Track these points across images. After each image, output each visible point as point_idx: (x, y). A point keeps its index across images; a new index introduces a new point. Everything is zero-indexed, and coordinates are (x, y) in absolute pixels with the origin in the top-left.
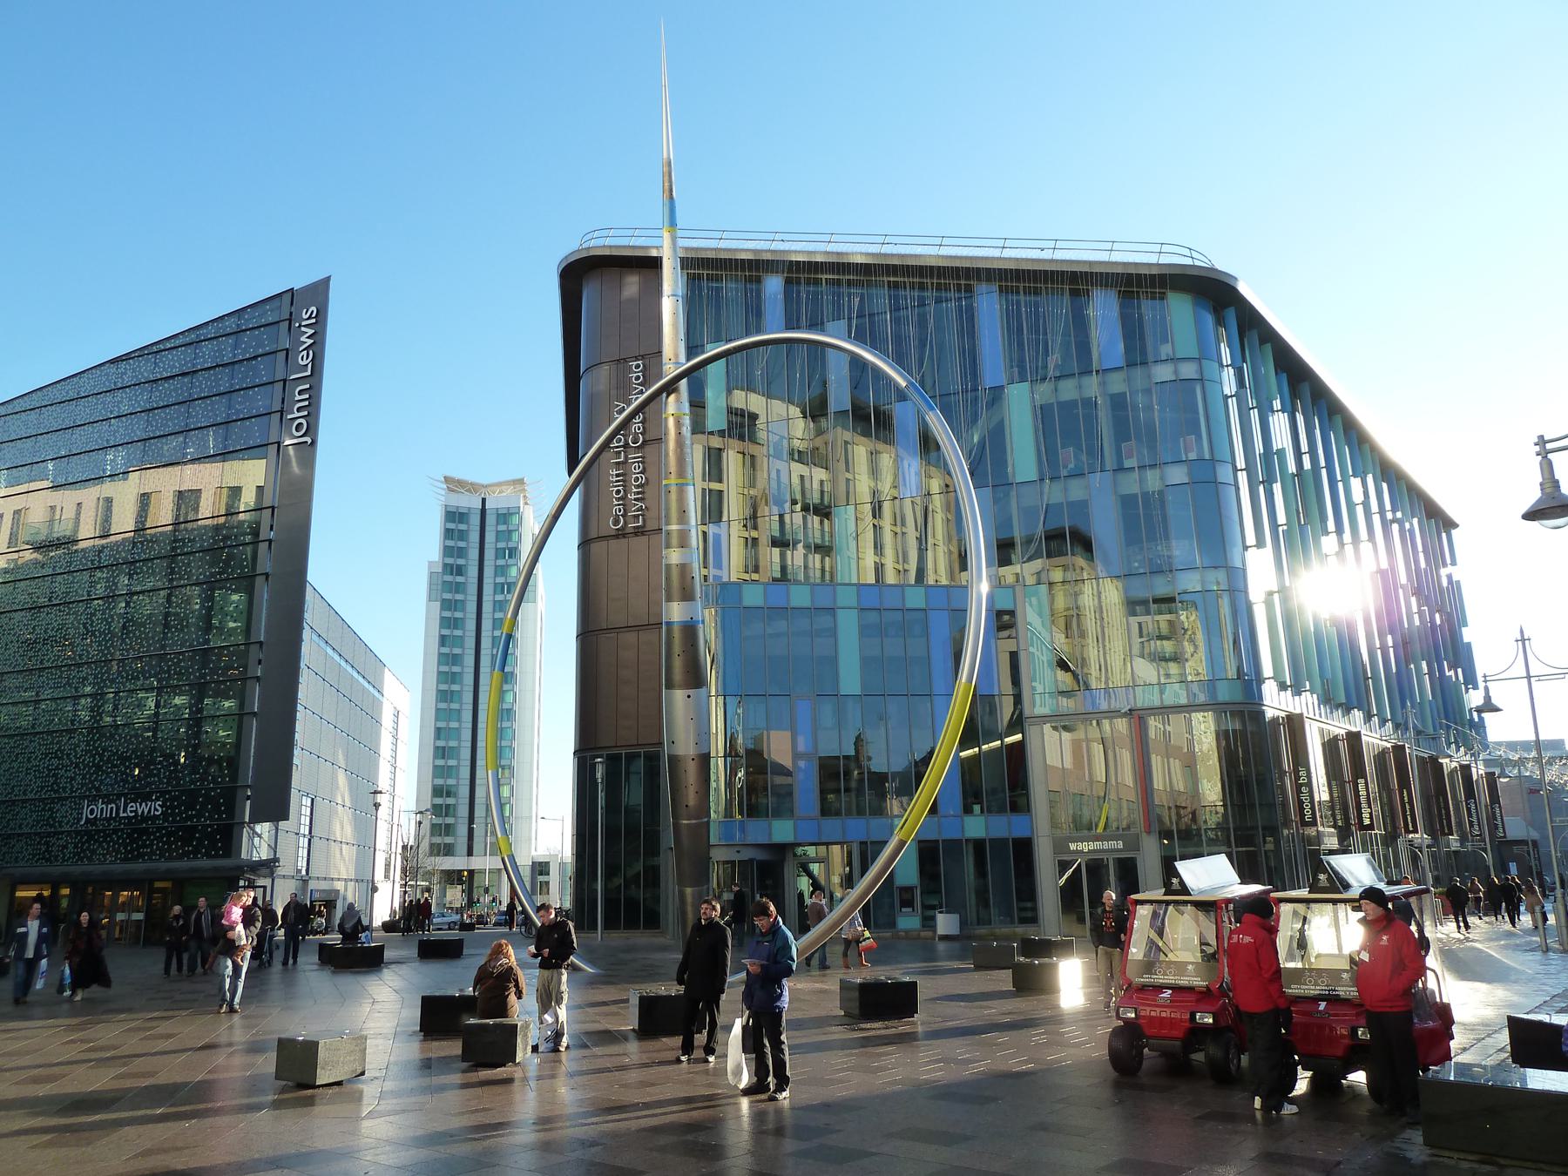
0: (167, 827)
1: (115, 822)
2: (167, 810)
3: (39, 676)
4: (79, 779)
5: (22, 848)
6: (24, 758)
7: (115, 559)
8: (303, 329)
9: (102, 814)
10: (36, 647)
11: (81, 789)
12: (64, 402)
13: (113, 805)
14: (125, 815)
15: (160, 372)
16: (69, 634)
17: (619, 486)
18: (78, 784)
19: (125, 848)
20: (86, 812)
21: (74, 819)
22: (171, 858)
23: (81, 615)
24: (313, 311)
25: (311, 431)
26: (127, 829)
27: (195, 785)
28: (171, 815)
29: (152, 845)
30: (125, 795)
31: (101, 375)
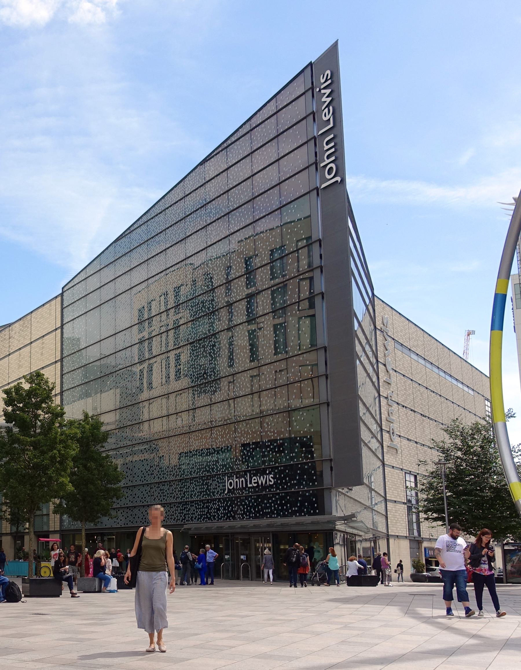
0: (278, 467)
1: (246, 491)
2: (277, 481)
10: (187, 485)
11: (223, 468)
12: (178, 222)
13: (243, 479)
14: (251, 485)
15: (235, 297)
16: (204, 453)
19: (254, 509)
20: (227, 484)
21: (221, 490)
22: (284, 516)
25: (340, 173)
26: (254, 496)
27: (294, 461)
28: (280, 484)
29: (271, 507)
31: (197, 218)
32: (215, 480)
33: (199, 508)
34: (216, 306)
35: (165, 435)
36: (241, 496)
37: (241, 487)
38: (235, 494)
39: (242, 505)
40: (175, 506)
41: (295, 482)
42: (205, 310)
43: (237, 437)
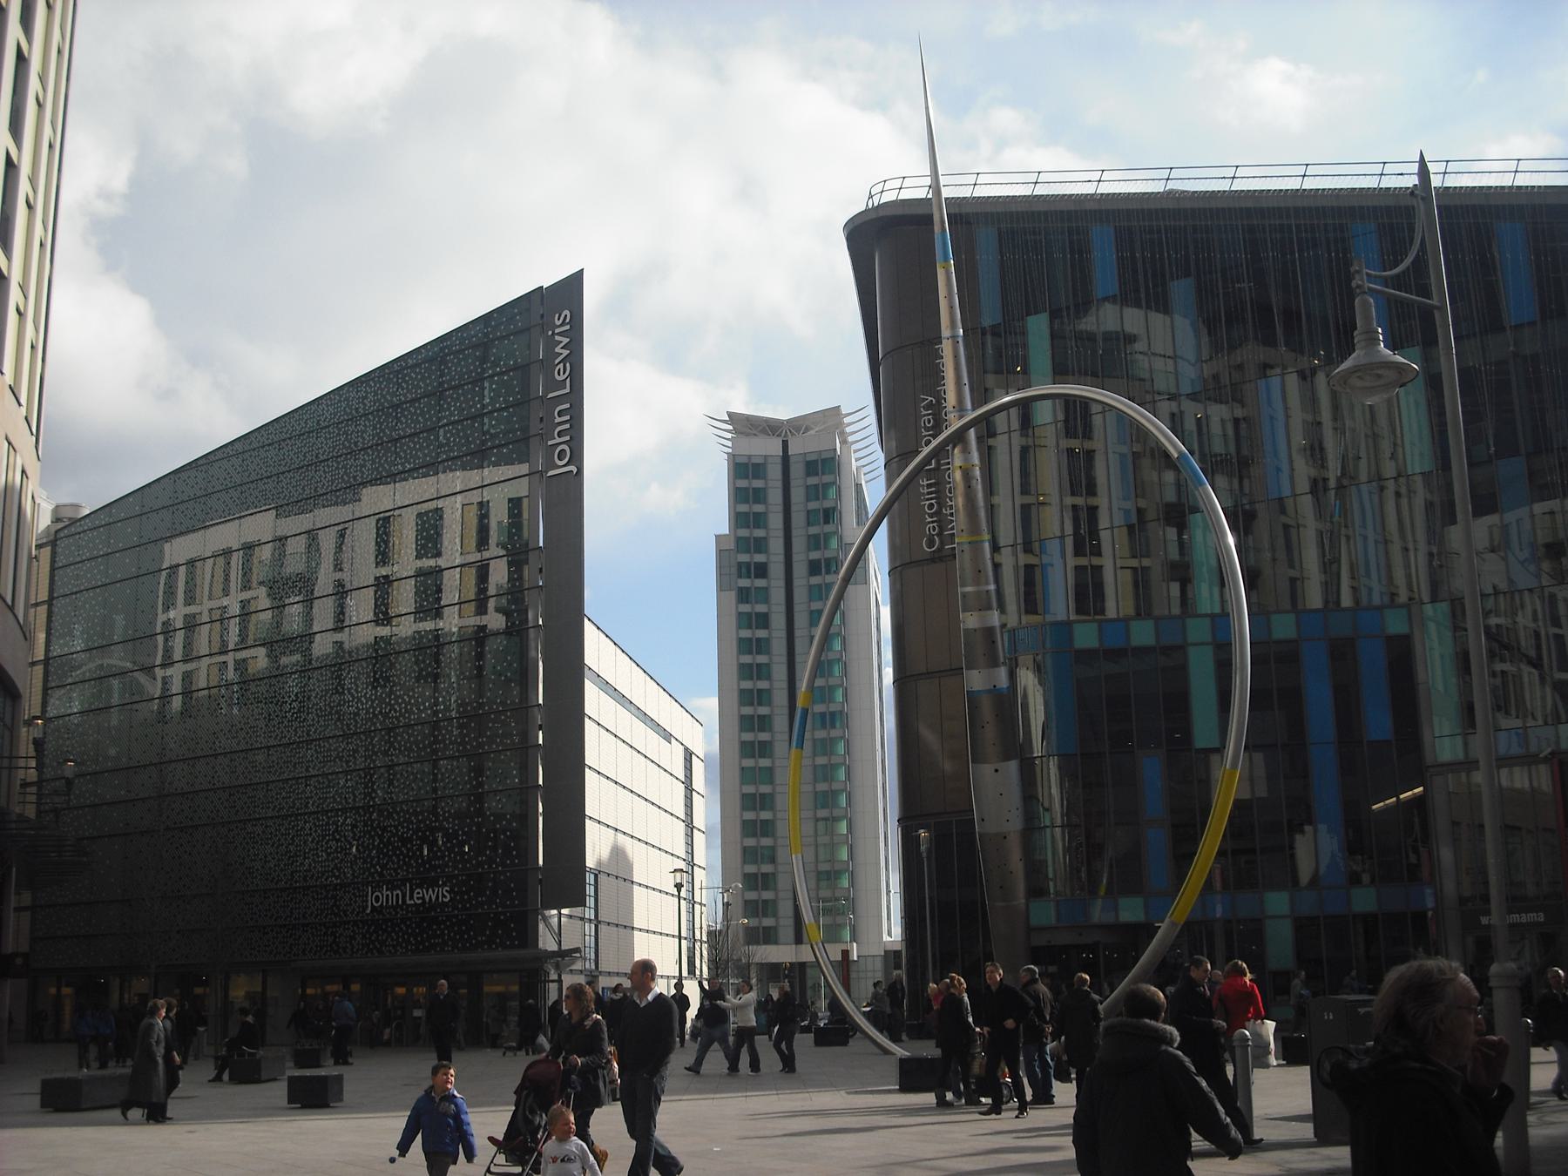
0: (458, 875)
3: (307, 749)
4: (359, 938)
5: (309, 939)
6: (303, 732)
7: (379, 473)
8: (557, 338)
9: (387, 902)
10: (300, 717)
16: (334, 701)
17: (931, 499)
18: (360, 832)
19: (417, 746)
20: (371, 900)
21: (359, 907)
23: (341, 826)
24: (566, 316)
27: (483, 868)
30: (410, 880)
32: (349, 892)
33: (320, 789)
34: (367, 476)
35: (261, 743)
36: (394, 880)
37: (394, 903)
38: (384, 915)
39: (395, 854)
40: (273, 895)
41: (484, 938)
42: (351, 412)
43: (399, 429)
